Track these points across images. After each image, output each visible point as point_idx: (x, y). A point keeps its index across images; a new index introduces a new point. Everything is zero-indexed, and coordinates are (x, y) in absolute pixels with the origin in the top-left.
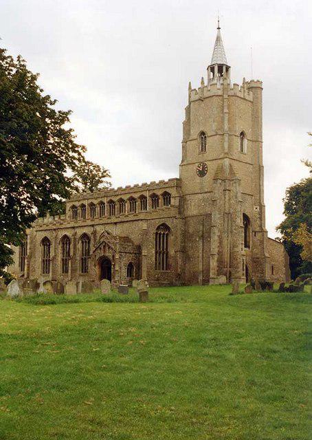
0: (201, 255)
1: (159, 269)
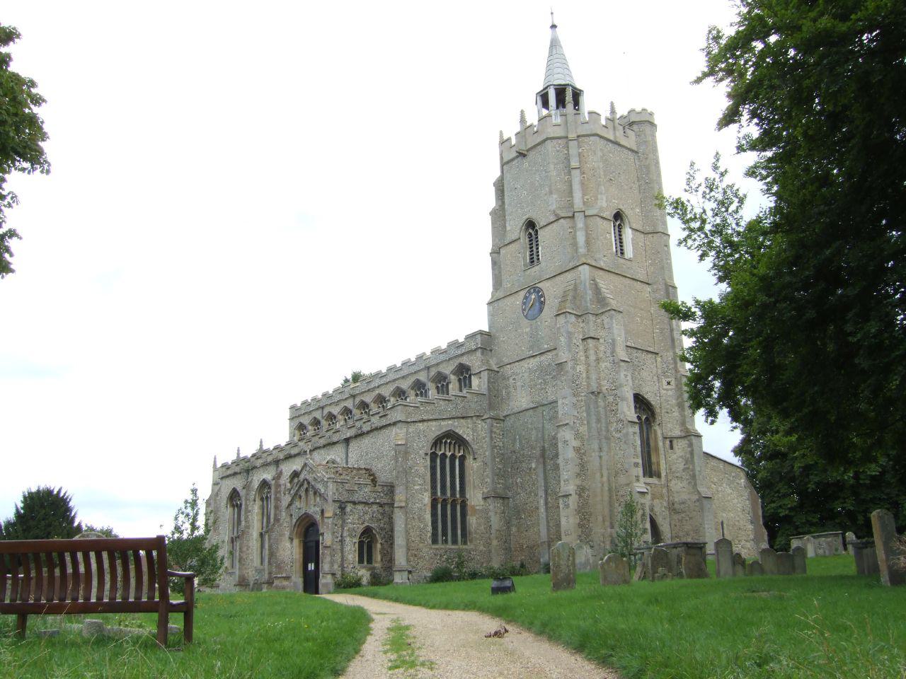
0: (542, 502)
1: (446, 542)
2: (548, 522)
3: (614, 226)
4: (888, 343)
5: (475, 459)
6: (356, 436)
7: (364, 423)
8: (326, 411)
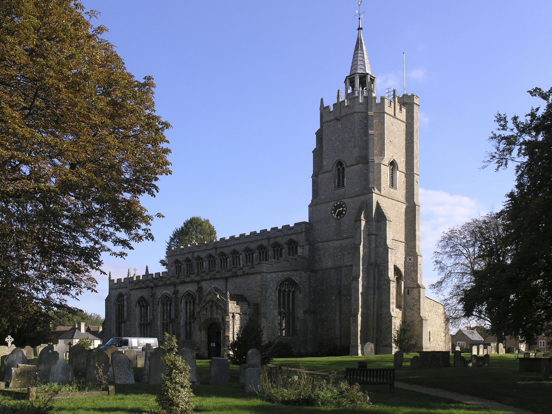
0: (338, 317)
2: (340, 328)
3: (390, 169)
4: (532, 133)
5: (300, 293)
6: (233, 277)
7: (238, 270)
8: (196, 254)
